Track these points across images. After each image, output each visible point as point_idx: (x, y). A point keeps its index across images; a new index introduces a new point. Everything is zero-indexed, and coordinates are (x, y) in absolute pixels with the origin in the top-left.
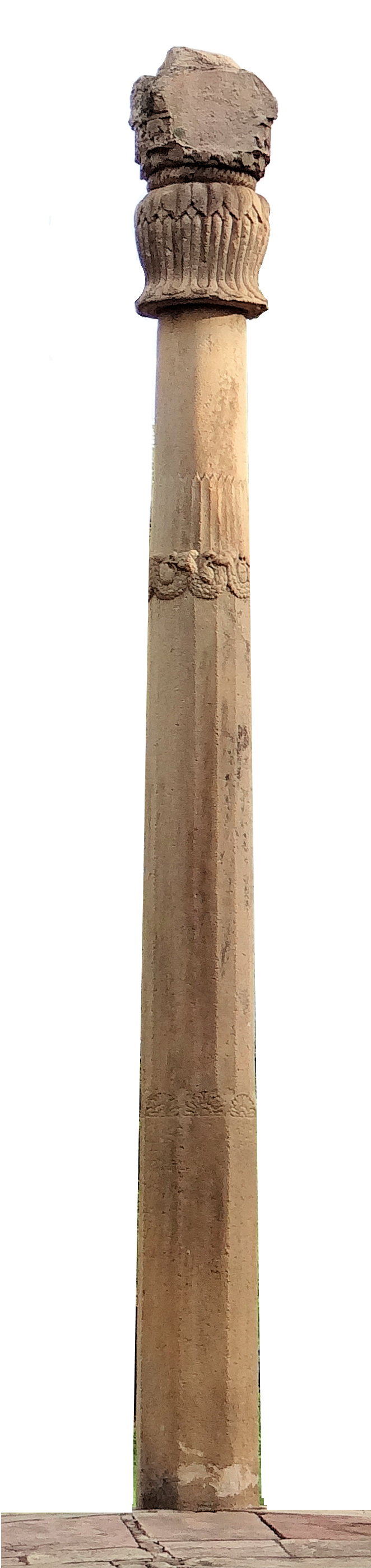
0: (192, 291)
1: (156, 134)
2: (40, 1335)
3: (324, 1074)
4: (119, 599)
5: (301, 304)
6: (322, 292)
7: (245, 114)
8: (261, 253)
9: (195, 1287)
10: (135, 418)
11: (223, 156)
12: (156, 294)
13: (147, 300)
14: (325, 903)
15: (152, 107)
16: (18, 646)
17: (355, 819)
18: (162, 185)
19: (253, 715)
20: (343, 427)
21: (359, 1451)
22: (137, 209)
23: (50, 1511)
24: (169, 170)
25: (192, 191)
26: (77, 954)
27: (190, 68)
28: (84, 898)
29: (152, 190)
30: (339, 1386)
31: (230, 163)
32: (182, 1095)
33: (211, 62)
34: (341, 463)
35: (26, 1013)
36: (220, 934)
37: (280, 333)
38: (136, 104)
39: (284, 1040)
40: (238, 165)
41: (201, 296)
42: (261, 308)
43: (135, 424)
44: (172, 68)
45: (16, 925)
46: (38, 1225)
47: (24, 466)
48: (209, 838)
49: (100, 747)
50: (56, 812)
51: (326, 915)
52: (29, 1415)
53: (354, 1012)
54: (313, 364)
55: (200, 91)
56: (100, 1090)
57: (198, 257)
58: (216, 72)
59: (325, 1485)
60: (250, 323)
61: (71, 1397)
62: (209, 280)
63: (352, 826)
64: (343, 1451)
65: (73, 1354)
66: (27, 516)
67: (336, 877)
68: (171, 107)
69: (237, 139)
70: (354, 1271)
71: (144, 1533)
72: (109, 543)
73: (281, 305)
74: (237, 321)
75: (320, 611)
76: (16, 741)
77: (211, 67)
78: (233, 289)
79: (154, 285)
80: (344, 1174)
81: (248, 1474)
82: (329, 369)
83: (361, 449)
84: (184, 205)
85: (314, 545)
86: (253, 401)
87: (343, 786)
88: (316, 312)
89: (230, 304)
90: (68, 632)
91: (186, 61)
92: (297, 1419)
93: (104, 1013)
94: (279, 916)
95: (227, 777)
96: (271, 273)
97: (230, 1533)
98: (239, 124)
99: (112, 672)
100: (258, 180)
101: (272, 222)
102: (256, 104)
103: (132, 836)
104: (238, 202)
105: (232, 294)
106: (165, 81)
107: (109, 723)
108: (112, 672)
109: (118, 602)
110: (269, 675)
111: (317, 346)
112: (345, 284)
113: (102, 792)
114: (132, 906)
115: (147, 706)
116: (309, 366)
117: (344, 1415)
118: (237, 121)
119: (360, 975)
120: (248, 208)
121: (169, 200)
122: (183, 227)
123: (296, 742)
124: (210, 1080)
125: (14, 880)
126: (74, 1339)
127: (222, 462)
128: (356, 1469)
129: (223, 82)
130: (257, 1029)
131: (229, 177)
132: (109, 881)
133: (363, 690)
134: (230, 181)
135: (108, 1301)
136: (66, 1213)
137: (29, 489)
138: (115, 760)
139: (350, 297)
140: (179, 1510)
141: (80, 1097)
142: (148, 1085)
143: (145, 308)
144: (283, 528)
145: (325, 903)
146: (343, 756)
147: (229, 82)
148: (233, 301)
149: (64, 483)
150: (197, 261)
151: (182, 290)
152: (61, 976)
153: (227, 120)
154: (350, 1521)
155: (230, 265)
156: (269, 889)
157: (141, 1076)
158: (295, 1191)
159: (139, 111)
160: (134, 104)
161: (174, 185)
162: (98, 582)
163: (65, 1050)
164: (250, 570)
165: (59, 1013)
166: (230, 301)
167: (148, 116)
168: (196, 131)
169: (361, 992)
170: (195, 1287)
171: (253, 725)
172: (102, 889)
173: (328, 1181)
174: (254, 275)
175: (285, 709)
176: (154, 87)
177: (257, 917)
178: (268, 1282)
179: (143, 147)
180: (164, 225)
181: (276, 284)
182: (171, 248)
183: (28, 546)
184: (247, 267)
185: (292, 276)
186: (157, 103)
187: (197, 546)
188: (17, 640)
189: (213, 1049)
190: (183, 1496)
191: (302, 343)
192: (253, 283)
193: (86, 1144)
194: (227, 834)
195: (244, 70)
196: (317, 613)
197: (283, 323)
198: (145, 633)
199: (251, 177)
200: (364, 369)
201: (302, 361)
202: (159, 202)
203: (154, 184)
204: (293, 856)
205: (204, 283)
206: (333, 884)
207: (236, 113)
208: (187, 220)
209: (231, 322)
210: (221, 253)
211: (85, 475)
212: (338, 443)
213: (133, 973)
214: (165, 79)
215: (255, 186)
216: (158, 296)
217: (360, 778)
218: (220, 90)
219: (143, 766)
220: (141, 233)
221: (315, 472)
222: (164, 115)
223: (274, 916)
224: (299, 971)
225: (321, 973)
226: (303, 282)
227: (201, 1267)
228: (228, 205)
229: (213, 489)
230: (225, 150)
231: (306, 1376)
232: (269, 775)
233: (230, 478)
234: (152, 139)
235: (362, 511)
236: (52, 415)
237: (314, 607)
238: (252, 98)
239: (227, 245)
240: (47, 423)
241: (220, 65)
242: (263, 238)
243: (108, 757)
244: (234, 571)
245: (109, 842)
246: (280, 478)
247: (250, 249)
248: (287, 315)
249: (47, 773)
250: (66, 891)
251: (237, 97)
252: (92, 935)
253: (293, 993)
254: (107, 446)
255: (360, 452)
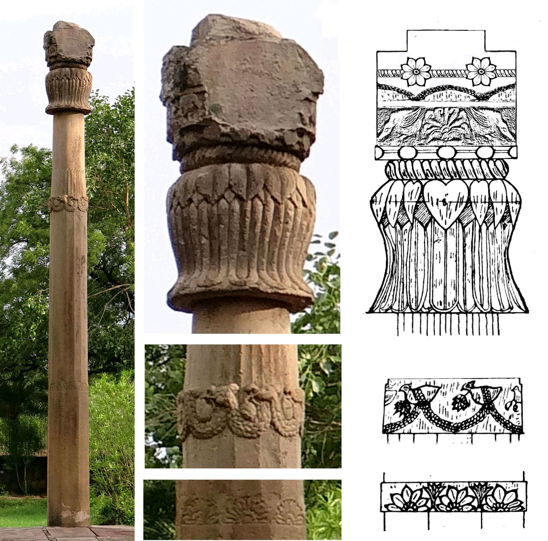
1: (190, 110)
2: (14, 466)
3: (112, 376)
5: (103, 110)
6: (110, 106)
8: (306, 240)
9: (67, 449)
10: (46, 149)
11: (263, 133)
13: (181, 292)
18: (55, 69)
19: (87, 252)
20: (118, 152)
24: (205, 149)
25: (229, 173)
27: (227, 37)
29: (186, 171)
31: (271, 141)
32: (62, 383)
33: (250, 31)
34: (117, 164)
35: (8, 355)
36: (75, 327)
38: (168, 77)
39: (98, 364)
40: (280, 144)
41: (240, 288)
42: (306, 301)
44: (208, 38)
46: (13, 428)
48: (72, 294)
51: (113, 321)
52: (10, 494)
54: (107, 130)
55: (238, 62)
56: (34, 381)
57: (67, 93)
58: (256, 42)
60: (85, 116)
61: (25, 487)
62: (249, 271)
64: (119, 506)
66: (8, 183)
67: (116, 308)
68: (206, 81)
69: (279, 115)
72: (37, 193)
73: (328, 297)
74: (280, 315)
76: (5, 261)
77: (250, 36)
78: (276, 280)
79: (188, 276)
80: (119, 411)
81: (86, 514)
82: (113, 132)
83: (124, 160)
84: (221, 188)
85: (107, 193)
86: (86, 143)
87: (118, 276)
89: (272, 297)
91: (223, 30)
92: (103, 495)
94: (96, 321)
97: (79, 534)
98: (282, 99)
99: (38, 237)
100: (302, 160)
101: (317, 206)
102: (300, 77)
104: (280, 184)
105: (274, 285)
106: (200, 52)
107: (37, 255)
109: (40, 213)
110: (92, 238)
112: (118, 103)
114: (45, 318)
118: (279, 96)
119: (124, 342)
121: (204, 182)
122: (220, 212)
124: (72, 378)
127: (76, 164)
128: (123, 512)
129: (263, 53)
131: (270, 157)
133: (125, 243)
134: (272, 161)
135: (37, 455)
137: (9, 174)
139: (120, 107)
140: (62, 527)
143: (49, 111)
146: (118, 266)
147: (270, 52)
149: (21, 172)
150: (236, 250)
151: (219, 281)
152: (21, 342)
155: (271, 253)
157: (48, 377)
158: (101, 416)
159: (171, 85)
160: (166, 77)
161: (209, 166)
162: (33, 206)
163: (22, 368)
166: (272, 293)
167: (181, 90)
168: (234, 106)
170: (67, 449)
172: (35, 312)
173: (113, 412)
174: (298, 264)
176: (187, 59)
177: (88, 321)
178: (92, 448)
179: (176, 125)
180: (55, 82)
181: (322, 275)
182: (207, 235)
184: (291, 256)
186: (190, 76)
187: (67, 194)
190: (63, 521)
192: (297, 274)
193: (29, 400)
194: (78, 293)
195: (286, 40)
197: (330, 317)
198: (49, 224)
199: (294, 158)
201: (104, 129)
202: (194, 185)
203: (187, 166)
204: (101, 300)
205: (244, 274)
206: (114, 310)
207: (278, 86)
209: (273, 317)
210: (262, 240)
211: (28, 169)
212: (116, 158)
213: (45, 341)
214: (56, 32)
215: (299, 167)
216: (193, 287)
217: (124, 274)
218: (260, 61)
219: (49, 271)
220: (173, 219)
221: (108, 168)
222: (198, 90)
223: (94, 321)
224: (103, 340)
225: (111, 341)
226: (104, 102)
228: (269, 187)
229: (73, 174)
230: (76, 56)
232: (93, 273)
234: (186, 116)
235: (124, 181)
238: (295, 71)
239: (269, 231)
242: (308, 224)
243: (37, 267)
245: (37, 296)
247: (294, 236)
248: (335, 309)
249: (15, 272)
251: (279, 69)
252: (31, 328)
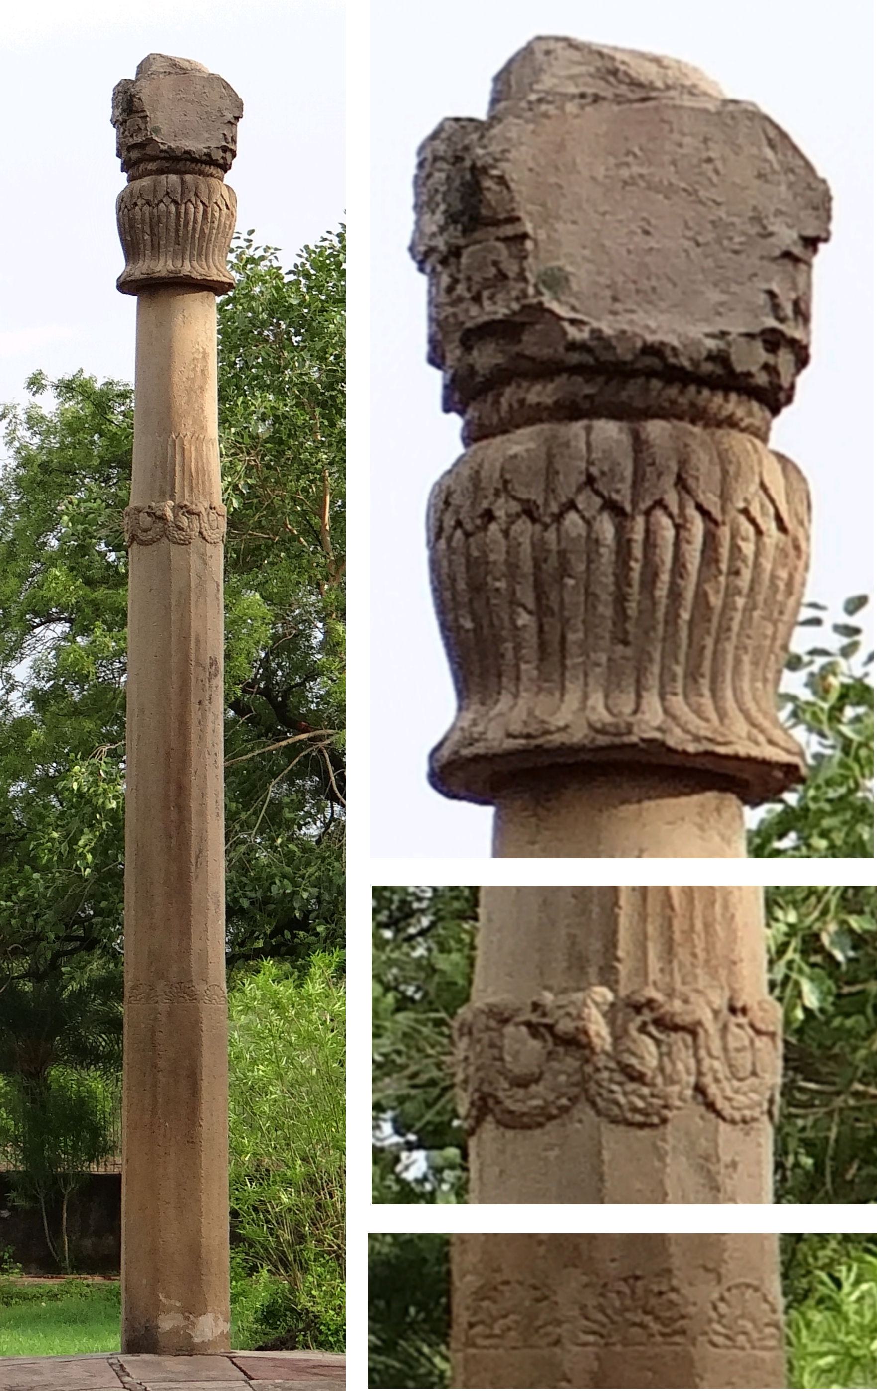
0: (591, 726)
2: (35, 1199)
3: (287, 966)
4: (103, 545)
5: (264, 282)
6: (283, 272)
7: (740, 227)
8: (786, 618)
10: (118, 384)
11: (676, 343)
12: (490, 735)
13: (466, 752)
14: (287, 814)
15: (476, 208)
16: (14, 587)
17: (313, 739)
19: (222, 647)
20: (302, 391)
21: (319, 1301)
22: (434, 494)
23: (44, 1355)
24: (525, 384)
25: (589, 444)
26: (68, 859)
27: (583, 96)
28: (73, 811)
29: (476, 440)
30: (301, 1243)
31: (696, 363)
32: (161, 985)
33: (642, 79)
34: (300, 423)
36: (194, 842)
37: (839, 842)
38: (431, 198)
39: (251, 936)
40: (719, 370)
41: (617, 740)
42: (786, 774)
43: (117, 388)
44: (533, 97)
45: (13, 835)
46: (33, 1102)
47: (19, 427)
48: (185, 757)
49: (87, 676)
50: (48, 734)
51: (289, 824)
52: (26, 1270)
53: (313, 911)
54: (275, 335)
55: (612, 161)
56: (88, 981)
57: (172, 240)
58: (656, 109)
59: (288, 1331)
60: (219, 299)
61: (63, 1254)
63: (311, 746)
64: (304, 1301)
65: (65, 1216)
66: (21, 472)
67: (297, 791)
68: (530, 207)
70: (314, 1141)
71: (128, 1375)
72: (94, 495)
73: (842, 765)
75: (282, 554)
76: (13, 671)
77: (640, 94)
78: (707, 720)
79: (483, 709)
80: (305, 1055)
82: (290, 339)
83: (318, 410)
84: (160, 194)
85: (276, 496)
86: (221, 369)
87: (303, 710)
88: (278, 289)
89: (699, 763)
90: (58, 573)
91: (571, 77)
92: (264, 1273)
93: (92, 913)
94: (246, 826)
95: (200, 703)
96: (812, 675)
97: (204, 1374)
99: (97, 609)
101: (815, 530)
103: (115, 755)
105: (703, 733)
106: (513, 134)
108: (97, 610)
109: (103, 547)
110: (237, 612)
111: (278, 320)
112: (303, 264)
113: (89, 717)
114: (116, 817)
115: (129, 640)
116: (271, 338)
117: (305, 1270)
118: (716, 247)
119: (318, 878)
120: (217, 197)
121: (524, 468)
123: (261, 671)
124: (186, 972)
125: (11, 794)
126: (65, 1203)
127: (195, 422)
128: (316, 1317)
130: (227, 926)
131: (693, 405)
132: (96, 795)
133: (320, 625)
135: (94, 1169)
136: (58, 1090)
137: (23, 447)
138: (100, 688)
139: (307, 276)
140: (159, 1354)
141: (70, 987)
142: (130, 976)
143: (125, 286)
144: (249, 481)
145: (287, 814)
146: (303, 684)
147: (693, 135)
148: (708, 753)
149: (54, 442)
150: (606, 643)
151: (561, 724)
152: (53, 879)
153: (688, 244)
154: (311, 1364)
156: (237, 802)
157: (124, 968)
158: (261, 1070)
159: (439, 217)
160: (425, 198)
162: (85, 530)
163: (57, 946)
164: (220, 518)
165: (52, 913)
166: (697, 754)
167: (464, 232)
168: (600, 273)
169: (320, 893)
171: (223, 656)
172: (89, 802)
173: (291, 1060)
174: (765, 680)
175: (251, 642)
176: (480, 151)
177: (227, 826)
178: (237, 1151)
179: (451, 320)
180: (142, 212)
181: (826, 706)
182: (531, 606)
183: (22, 498)
184: (746, 659)
185: (256, 257)
186: (489, 195)
188: (13, 581)
189: (189, 944)
191: (265, 317)
192: (763, 704)
193: (76, 1029)
194: (200, 753)
196: (279, 556)
197: (848, 815)
199: (755, 406)
200: (320, 340)
201: (266, 333)
202: (497, 475)
203: (481, 426)
204: (258, 772)
206: (294, 797)
207: (713, 222)
208: (575, 525)
209: (700, 814)
210: (193, 237)
211: (73, 435)
214: (513, 128)
215: (768, 429)
216: (137, 275)
217: (318, 704)
218: (666, 158)
220: (445, 563)
221: (277, 431)
222: (509, 230)
223: (242, 826)
224: (264, 875)
225: (284, 876)
226: (266, 262)
227: (178, 1138)
228: (691, 482)
229: (187, 447)
230: (196, 146)
231: (272, 1235)
232: (238, 701)
233: (202, 436)
235: (319, 466)
236: (43, 382)
237: (276, 552)
238: (757, 182)
239: (689, 595)
240: (38, 388)
241: (668, 87)
242: (791, 577)
243: (95, 685)
244: (206, 519)
245: (95, 761)
246: (246, 436)
247: (754, 608)
248: (860, 794)
249: (39, 699)
250: (57, 804)
251: (715, 179)
252: (81, 843)
253: (259, 894)
254: (92, 408)
255: (317, 413)
